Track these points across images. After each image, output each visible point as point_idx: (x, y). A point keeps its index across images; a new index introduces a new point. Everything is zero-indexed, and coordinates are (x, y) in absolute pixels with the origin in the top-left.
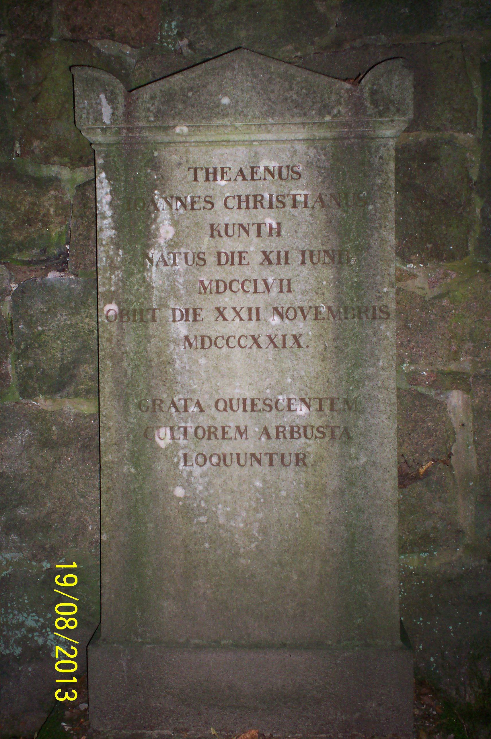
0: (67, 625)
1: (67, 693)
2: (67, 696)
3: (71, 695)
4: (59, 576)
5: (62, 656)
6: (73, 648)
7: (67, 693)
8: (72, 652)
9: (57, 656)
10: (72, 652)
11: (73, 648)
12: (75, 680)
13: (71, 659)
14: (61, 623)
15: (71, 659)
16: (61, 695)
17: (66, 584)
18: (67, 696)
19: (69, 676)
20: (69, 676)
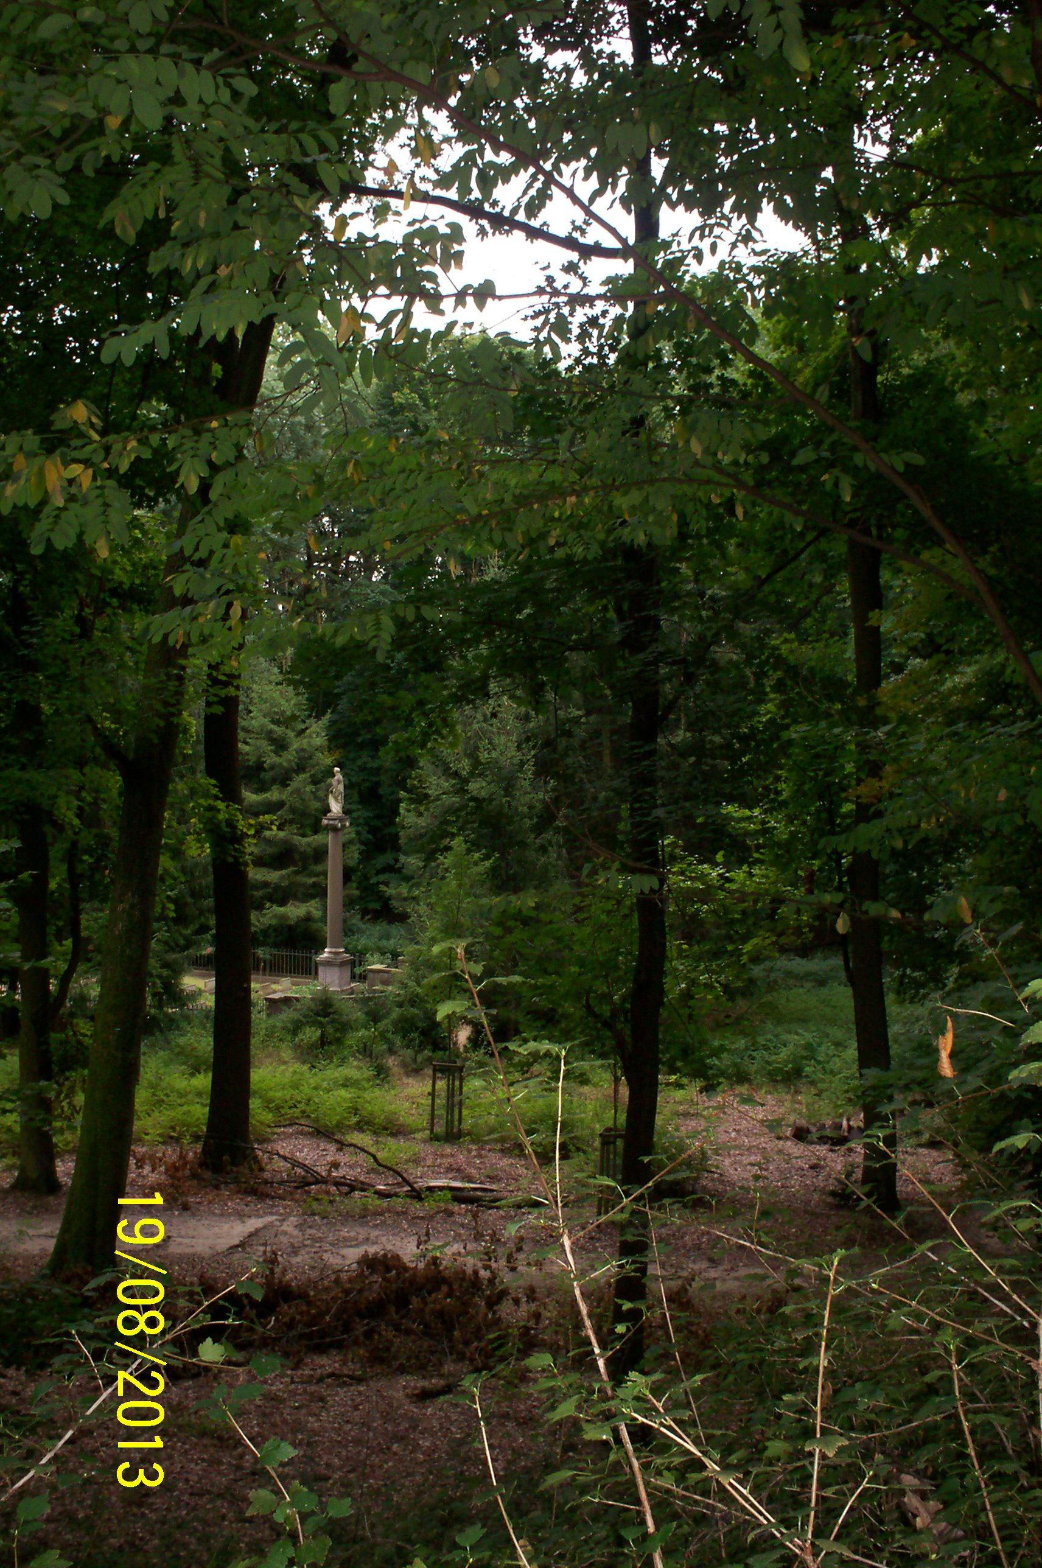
0: (142, 1326)
1: (141, 1471)
2: (141, 1477)
3: (152, 1476)
4: (126, 1465)
5: (131, 1392)
6: (154, 1374)
7: (141, 1471)
8: (154, 1384)
9: (120, 1393)
10: (154, 1384)
11: (154, 1374)
12: (158, 1443)
13: (153, 1399)
14: (130, 1323)
15: (153, 1399)
16: (130, 1475)
17: (140, 1240)
18: (141, 1477)
19: (147, 1434)
20: (147, 1434)
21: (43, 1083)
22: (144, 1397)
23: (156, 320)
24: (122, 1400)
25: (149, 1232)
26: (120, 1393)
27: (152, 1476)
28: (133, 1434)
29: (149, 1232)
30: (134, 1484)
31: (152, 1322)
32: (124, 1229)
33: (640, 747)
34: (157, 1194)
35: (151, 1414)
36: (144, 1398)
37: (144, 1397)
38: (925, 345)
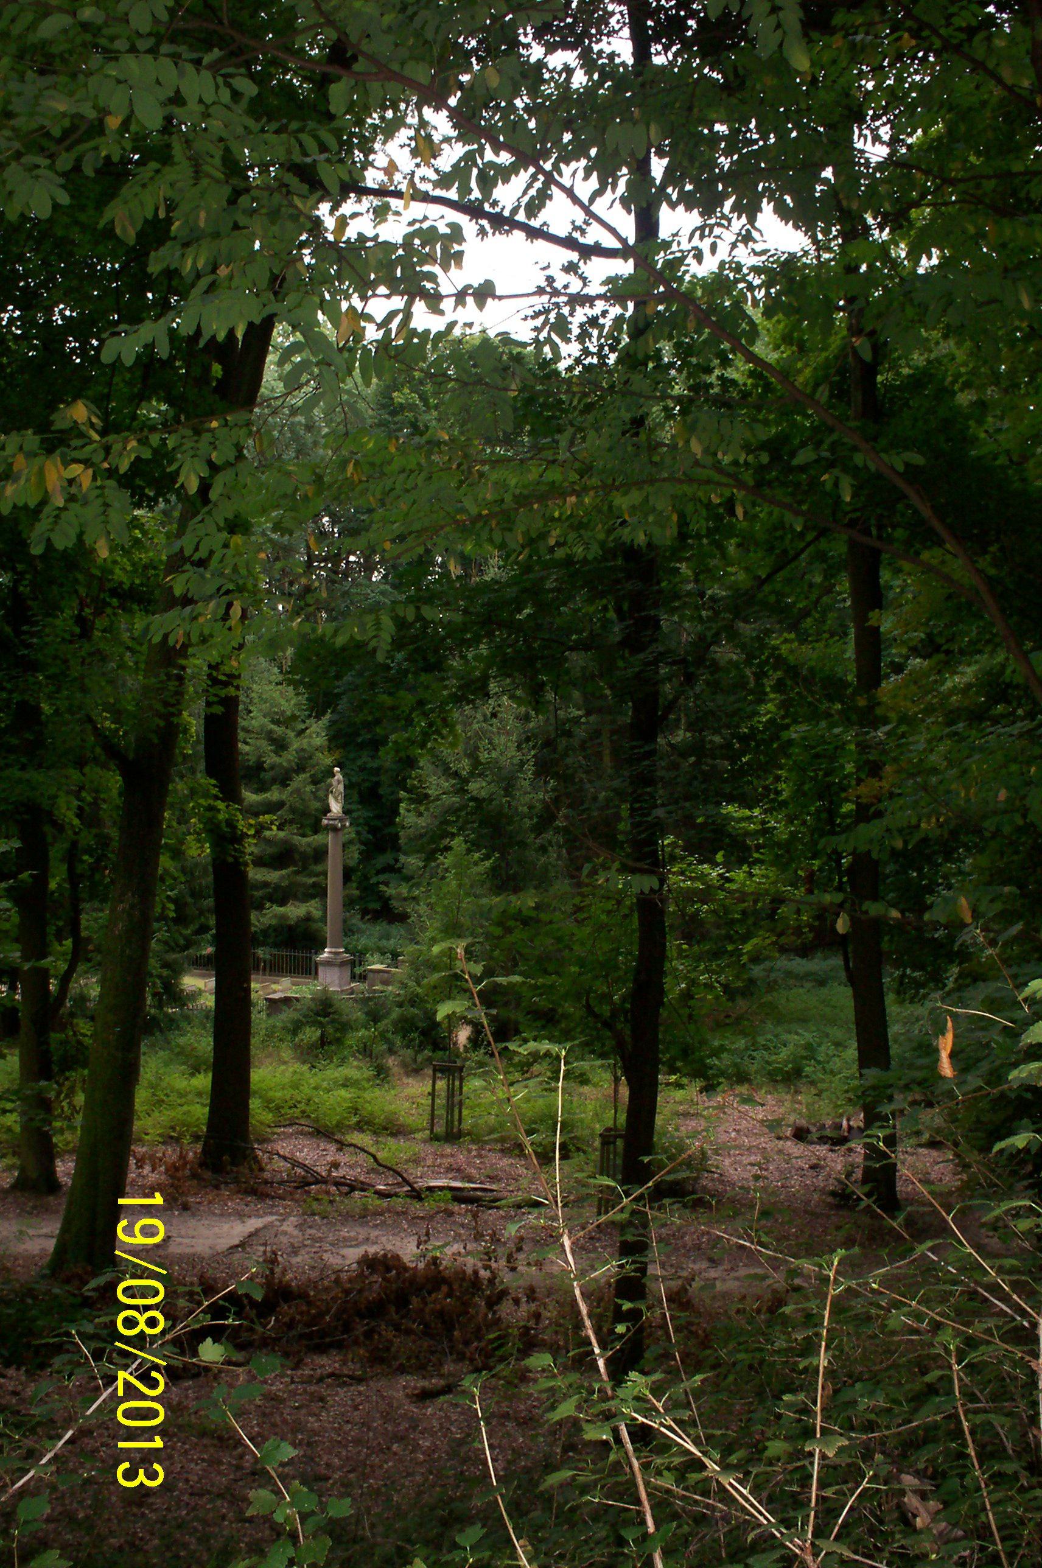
0: (142, 1326)
1: (141, 1471)
2: (141, 1477)
3: (152, 1476)
4: (126, 1465)
5: (131, 1392)
6: (154, 1374)
7: (141, 1471)
8: (154, 1384)
9: (120, 1393)
10: (154, 1384)
11: (154, 1374)
12: (158, 1443)
13: (153, 1399)
14: (130, 1323)
15: (153, 1399)
16: (130, 1475)
17: (140, 1240)
18: (141, 1477)
19: (147, 1434)
20: (147, 1434)
21: (43, 1083)
22: (144, 1397)
23: (156, 320)
24: (122, 1400)
25: (149, 1232)
26: (120, 1393)
27: (152, 1476)
28: (133, 1434)
29: (149, 1232)
30: (134, 1484)
31: (152, 1322)
32: (124, 1229)
33: (640, 747)
34: (157, 1194)
35: (151, 1414)
36: (144, 1398)
37: (144, 1397)
38: (925, 345)
